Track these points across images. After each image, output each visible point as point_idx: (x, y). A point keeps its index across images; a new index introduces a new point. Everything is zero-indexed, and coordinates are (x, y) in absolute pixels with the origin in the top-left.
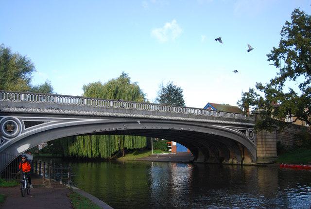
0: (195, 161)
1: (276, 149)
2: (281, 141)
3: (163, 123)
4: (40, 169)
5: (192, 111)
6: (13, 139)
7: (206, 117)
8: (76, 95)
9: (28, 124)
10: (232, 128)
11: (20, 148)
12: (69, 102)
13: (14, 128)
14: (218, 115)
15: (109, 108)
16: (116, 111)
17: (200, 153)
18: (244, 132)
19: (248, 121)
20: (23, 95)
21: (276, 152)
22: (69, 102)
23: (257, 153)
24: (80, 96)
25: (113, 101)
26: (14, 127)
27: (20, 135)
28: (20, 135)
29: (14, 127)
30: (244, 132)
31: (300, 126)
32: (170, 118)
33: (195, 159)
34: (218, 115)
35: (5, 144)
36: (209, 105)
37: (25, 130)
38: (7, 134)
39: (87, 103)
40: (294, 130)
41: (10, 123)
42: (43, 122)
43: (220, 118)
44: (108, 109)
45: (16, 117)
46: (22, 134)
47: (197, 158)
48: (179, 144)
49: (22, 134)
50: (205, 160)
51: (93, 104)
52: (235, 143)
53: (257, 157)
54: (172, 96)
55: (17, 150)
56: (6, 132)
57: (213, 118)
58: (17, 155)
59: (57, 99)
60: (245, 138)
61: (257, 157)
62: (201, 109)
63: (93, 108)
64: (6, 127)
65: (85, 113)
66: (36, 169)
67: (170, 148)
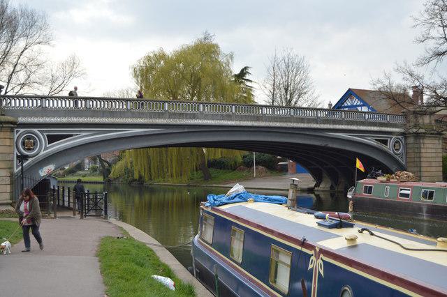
0: (316, 189)
1: (441, 169)
3: (285, 133)
4: (69, 198)
6: (34, 158)
7: (281, 119)
8: (103, 96)
9: (52, 139)
10: (361, 137)
12: (18, 105)
13: (35, 144)
17: (325, 175)
18: (385, 142)
21: (441, 174)
23: (151, 149)
25: (235, 105)
26: (27, 139)
27: (42, 153)
28: (42, 153)
30: (385, 142)
37: (48, 146)
38: (22, 149)
41: (29, 138)
42: (71, 136)
44: (160, 115)
45: (36, 130)
47: (320, 183)
54: (288, 90)
56: (25, 149)
58: (39, 179)
59: (15, 103)
63: (141, 115)
64: (23, 144)
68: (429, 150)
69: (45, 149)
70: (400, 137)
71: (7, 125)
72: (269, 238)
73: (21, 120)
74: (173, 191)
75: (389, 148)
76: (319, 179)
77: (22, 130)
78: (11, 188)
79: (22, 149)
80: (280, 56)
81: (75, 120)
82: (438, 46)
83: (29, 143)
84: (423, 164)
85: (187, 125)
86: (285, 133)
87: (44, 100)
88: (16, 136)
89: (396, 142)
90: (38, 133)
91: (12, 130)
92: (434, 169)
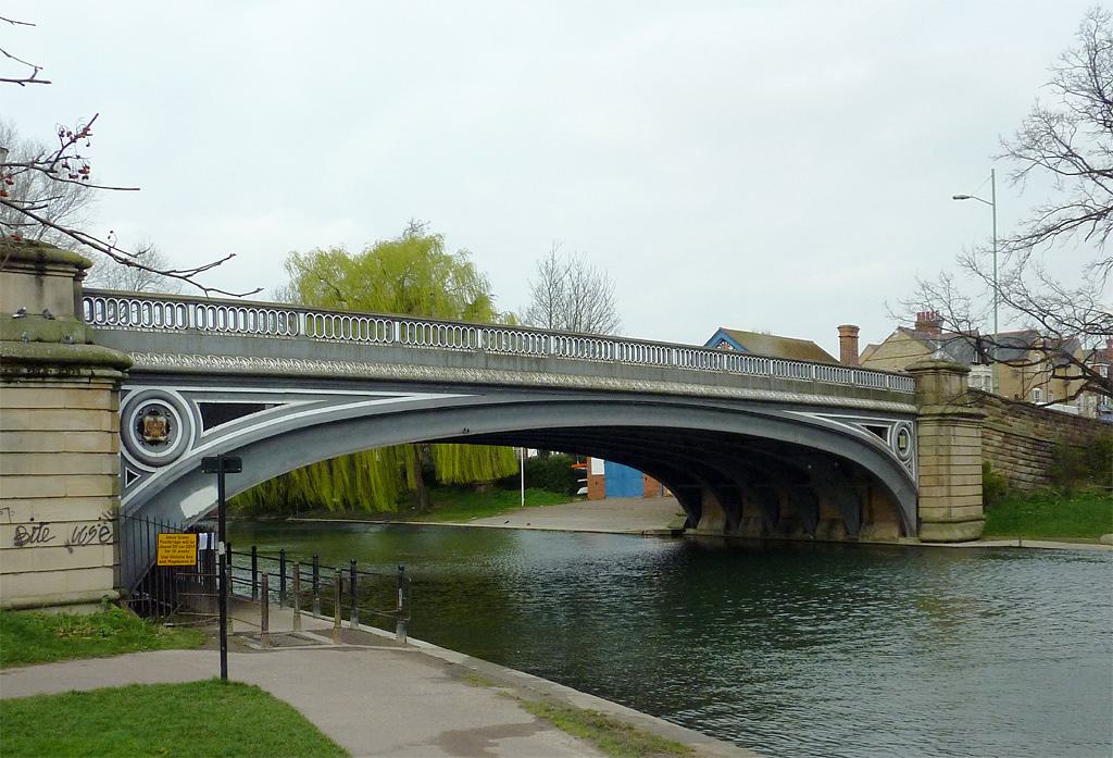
1: (980, 490)
2: (992, 461)
3: (638, 404)
5: (632, 354)
9: (214, 415)
11: (186, 501)
12: (231, 325)
14: (750, 369)
15: (470, 355)
16: (492, 363)
18: (880, 432)
19: (896, 397)
20: (397, 323)
21: (979, 500)
22: (231, 325)
24: (264, 297)
26: (168, 426)
27: (190, 453)
28: (190, 453)
29: (168, 426)
30: (880, 432)
31: (1075, 417)
32: (663, 387)
33: (688, 525)
34: (750, 369)
35: (136, 491)
36: (722, 336)
39: (403, 336)
40: (1033, 423)
41: (154, 411)
43: (847, 391)
44: (467, 357)
45: (172, 390)
46: (196, 451)
48: (614, 465)
49: (196, 451)
50: (728, 526)
51: (320, 333)
52: (846, 467)
53: (919, 520)
55: (179, 505)
56: (143, 442)
57: (789, 386)
60: (883, 455)
61: (919, 520)
62: (694, 348)
63: (422, 356)
64: (140, 427)
65: (287, 366)
66: (283, 584)
67: (584, 484)
68: (964, 451)
69: (195, 442)
70: (907, 422)
71: (106, 372)
72: (215, 404)
73: (140, 361)
74: (569, 582)
75: (889, 443)
76: (692, 505)
77: (136, 390)
78: (117, 556)
79: (141, 406)
80: (561, 263)
81: (273, 365)
82: (1038, 217)
83: (153, 427)
84: (955, 480)
85: (752, 400)
86: (659, 404)
87: (191, 307)
88: (122, 405)
89: (901, 434)
90: (180, 397)
91: (116, 388)
92: (969, 491)
